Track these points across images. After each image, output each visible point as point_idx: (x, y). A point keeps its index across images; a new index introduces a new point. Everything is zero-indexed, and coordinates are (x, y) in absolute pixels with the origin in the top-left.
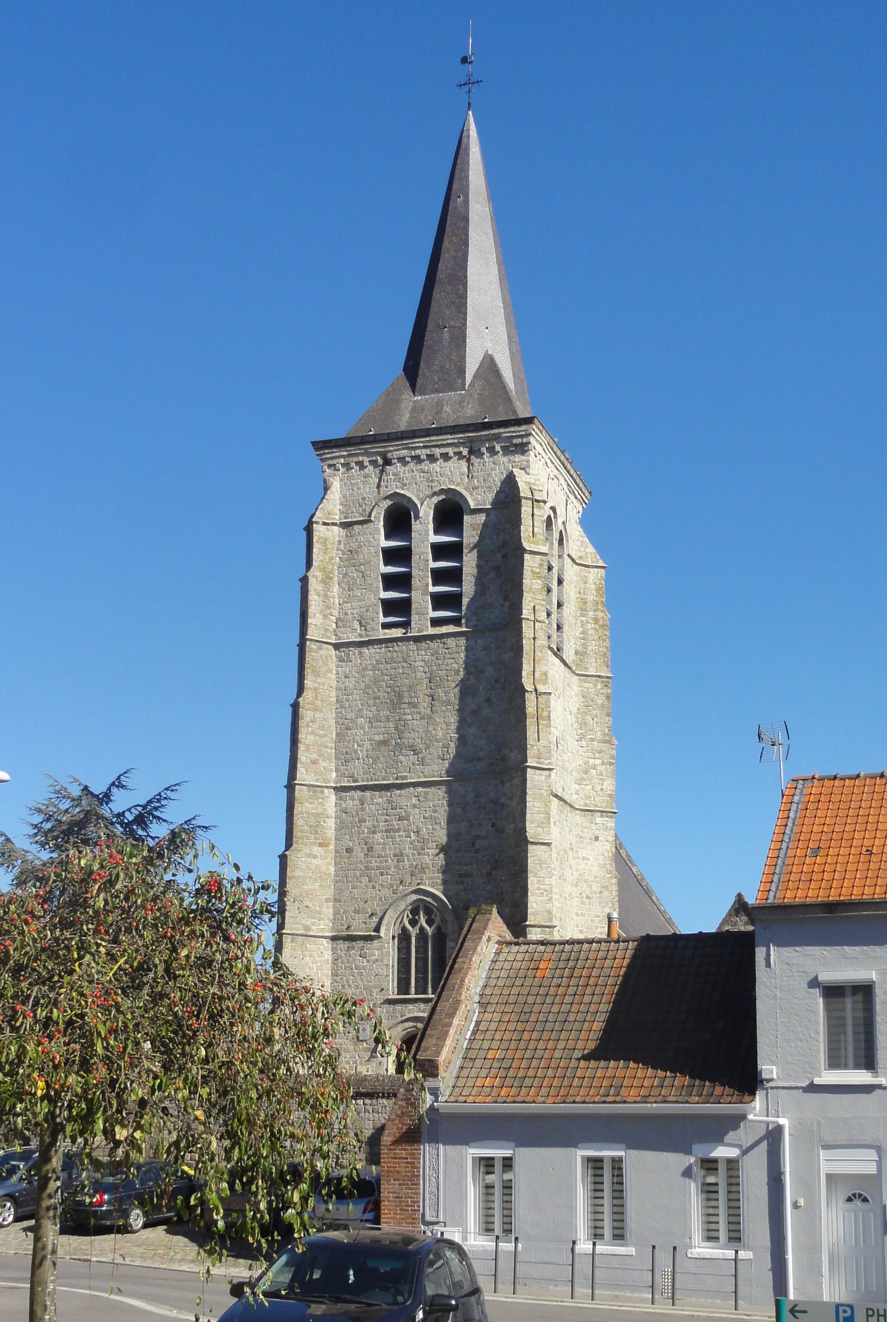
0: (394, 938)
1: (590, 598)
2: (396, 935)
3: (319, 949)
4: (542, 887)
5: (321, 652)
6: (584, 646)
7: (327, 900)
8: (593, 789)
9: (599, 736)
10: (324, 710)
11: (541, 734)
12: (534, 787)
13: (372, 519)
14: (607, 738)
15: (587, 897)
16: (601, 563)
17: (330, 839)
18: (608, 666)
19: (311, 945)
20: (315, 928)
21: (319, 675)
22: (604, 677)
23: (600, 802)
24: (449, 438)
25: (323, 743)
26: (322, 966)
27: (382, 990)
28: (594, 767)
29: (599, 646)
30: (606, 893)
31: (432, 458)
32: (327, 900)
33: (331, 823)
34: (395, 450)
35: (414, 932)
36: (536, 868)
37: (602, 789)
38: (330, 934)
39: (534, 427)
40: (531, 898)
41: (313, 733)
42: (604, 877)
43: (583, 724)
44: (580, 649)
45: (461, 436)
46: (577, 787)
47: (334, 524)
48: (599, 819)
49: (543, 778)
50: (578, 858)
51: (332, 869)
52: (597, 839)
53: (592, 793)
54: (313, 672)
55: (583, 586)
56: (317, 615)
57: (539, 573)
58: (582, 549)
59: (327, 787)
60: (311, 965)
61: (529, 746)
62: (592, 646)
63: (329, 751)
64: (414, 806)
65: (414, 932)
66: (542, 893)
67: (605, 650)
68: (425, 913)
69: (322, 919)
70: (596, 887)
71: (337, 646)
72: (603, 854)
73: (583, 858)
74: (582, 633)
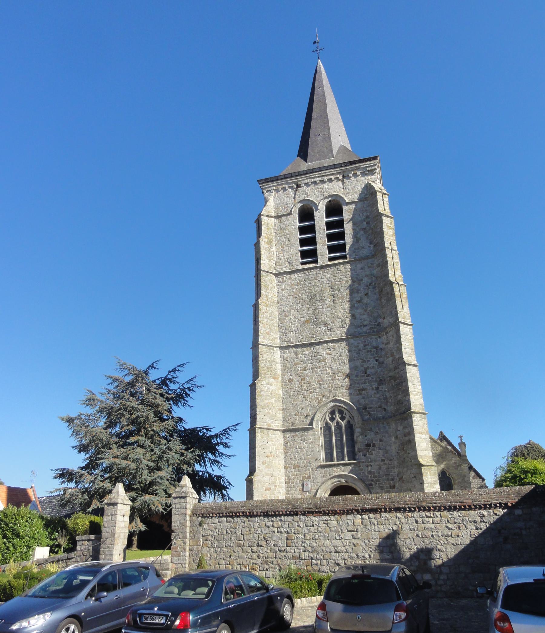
0: (321, 428)
19: (272, 434)
20: (273, 425)
24: (332, 171)
33: (279, 366)
41: (266, 318)
56: (266, 259)
65: (333, 425)
71: (277, 275)
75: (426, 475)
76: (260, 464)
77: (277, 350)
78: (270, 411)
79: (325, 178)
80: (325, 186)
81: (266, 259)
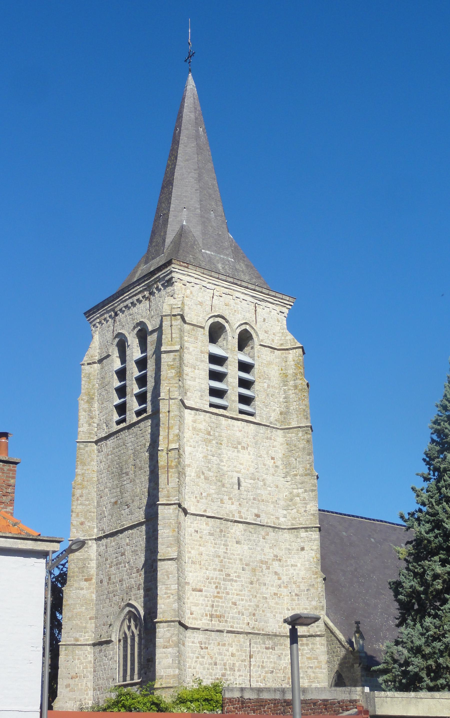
0: (120, 641)
1: (290, 372)
2: (121, 638)
3: (84, 653)
4: (169, 592)
5: (87, 449)
6: (287, 408)
7: (91, 619)
8: (298, 512)
9: (301, 471)
10: (88, 487)
11: (170, 479)
12: (164, 518)
13: (110, 354)
14: (308, 472)
15: (296, 595)
16: (299, 345)
17: (93, 575)
18: (307, 418)
19: (78, 651)
20: (82, 639)
21: (85, 465)
22: (304, 427)
23: (305, 521)
24: (139, 288)
25: (88, 510)
26: (86, 666)
27: (114, 679)
28: (298, 495)
29: (299, 405)
30: (312, 590)
31: (133, 304)
32: (91, 619)
33: (93, 564)
34: (118, 305)
35: (129, 634)
36: (163, 578)
37: (305, 511)
38: (91, 642)
39: (173, 266)
40: (160, 601)
41: (81, 504)
42: (311, 578)
43: (288, 465)
44: (284, 410)
45: (143, 284)
46: (285, 512)
47: (94, 363)
48: (303, 534)
49: (171, 511)
50: (287, 566)
51: (94, 596)
52: (303, 549)
53: (297, 515)
54: (81, 463)
55: (283, 364)
56: (85, 425)
57: (173, 365)
58: (283, 338)
59: (90, 540)
60: (78, 665)
61: (160, 490)
62: (293, 406)
63: (92, 514)
64: (127, 545)
65: (129, 634)
66: (169, 597)
67: (304, 407)
68: (135, 621)
69: (87, 632)
70: (303, 587)
71: (96, 442)
72: (308, 560)
73: (292, 565)
74: (285, 398)
75: (63, 708)
76: (62, 688)
77: (92, 543)
78: (79, 623)
79: (128, 302)
80: (134, 310)
81: (85, 425)
